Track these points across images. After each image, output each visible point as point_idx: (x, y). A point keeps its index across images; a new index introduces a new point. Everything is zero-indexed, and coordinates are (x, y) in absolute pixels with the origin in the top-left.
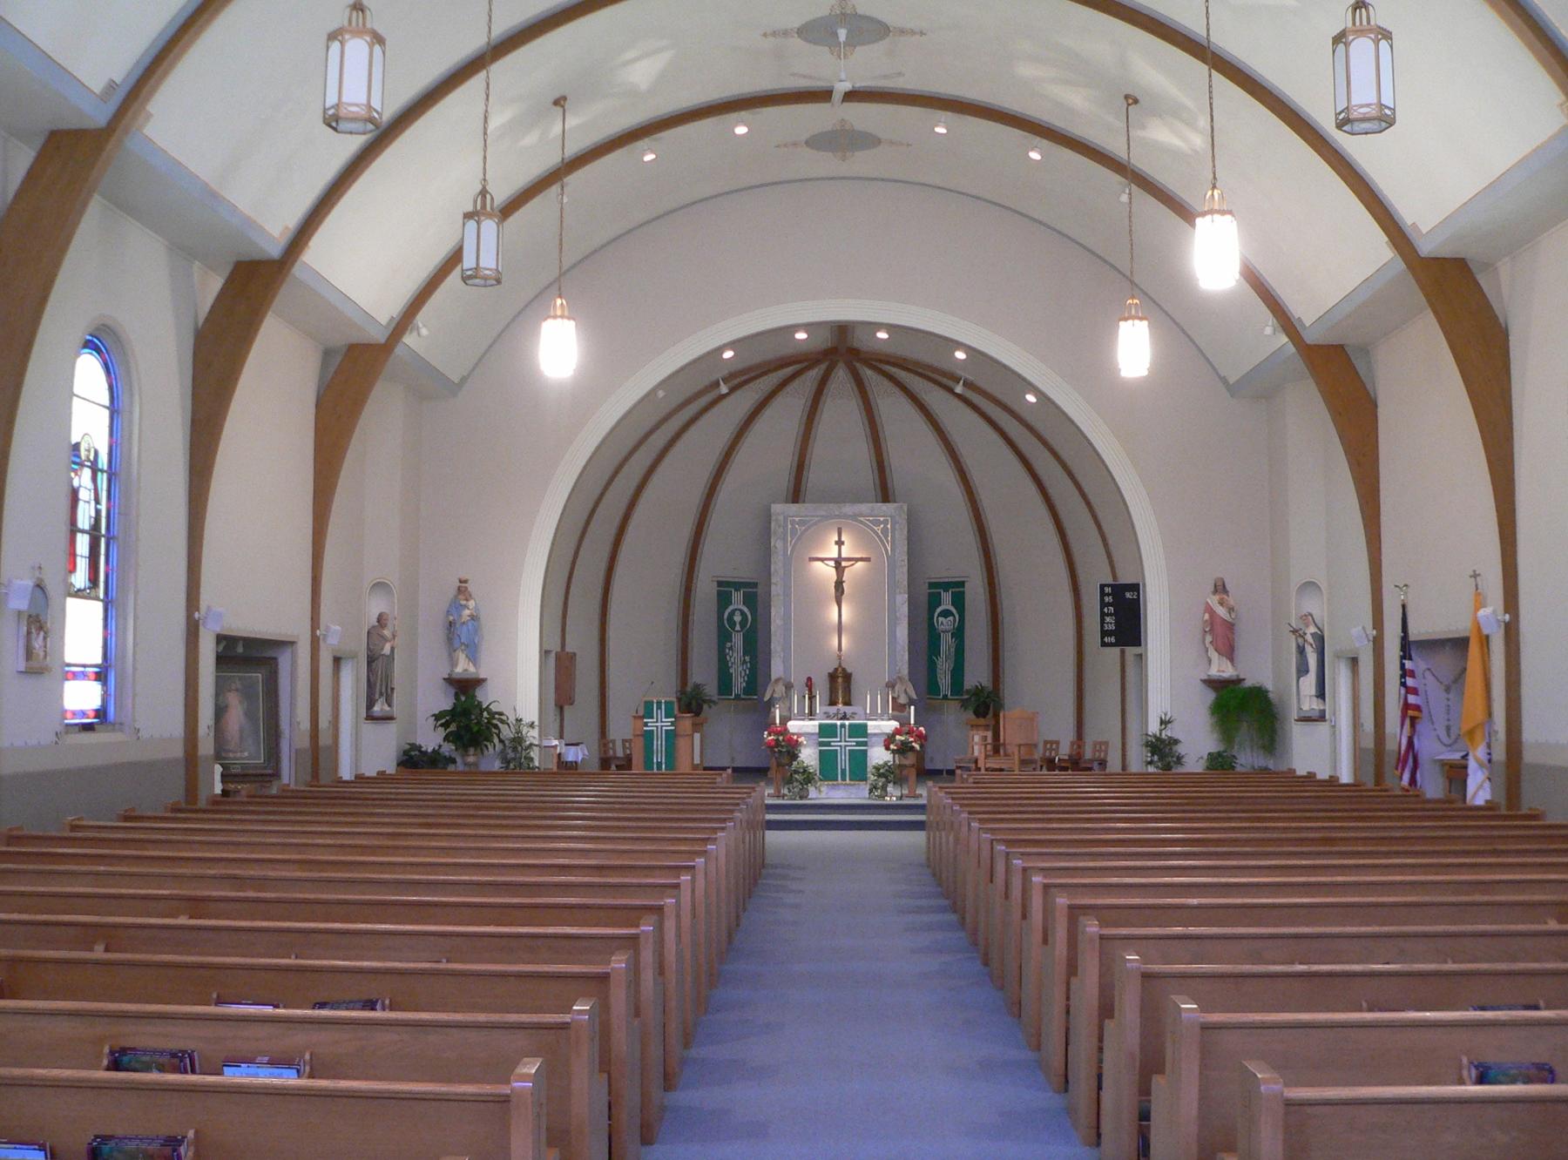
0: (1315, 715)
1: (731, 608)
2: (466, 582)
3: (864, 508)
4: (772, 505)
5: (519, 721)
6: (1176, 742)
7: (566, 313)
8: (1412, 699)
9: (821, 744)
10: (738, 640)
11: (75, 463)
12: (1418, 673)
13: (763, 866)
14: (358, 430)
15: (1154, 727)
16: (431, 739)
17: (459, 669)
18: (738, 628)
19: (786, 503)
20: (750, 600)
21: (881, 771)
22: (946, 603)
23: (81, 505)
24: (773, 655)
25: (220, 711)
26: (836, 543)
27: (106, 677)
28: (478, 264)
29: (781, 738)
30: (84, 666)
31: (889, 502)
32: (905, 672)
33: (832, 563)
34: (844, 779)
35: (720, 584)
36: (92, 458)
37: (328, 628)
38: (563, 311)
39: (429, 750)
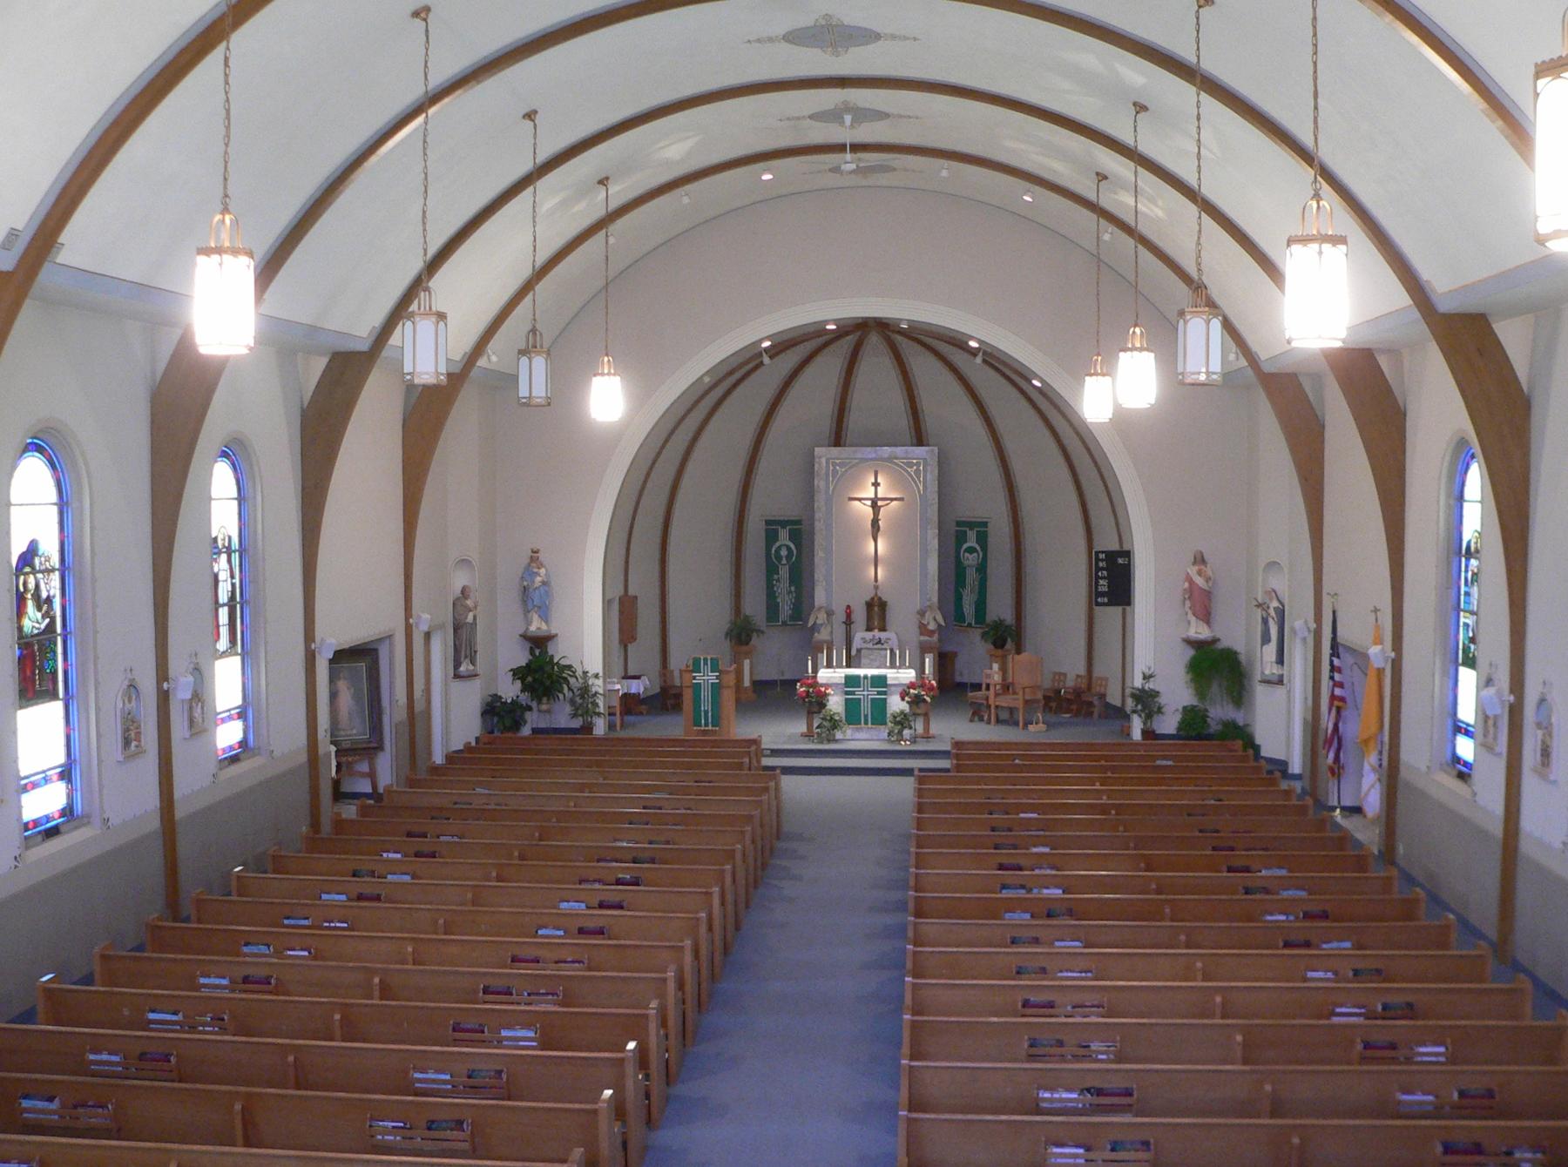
0: (1275, 679)
1: (778, 544)
2: (537, 552)
3: (899, 450)
4: (816, 449)
5: (585, 673)
6: (1157, 694)
7: (612, 371)
8: (1338, 692)
9: (847, 693)
10: (784, 572)
11: (215, 554)
12: (1346, 671)
13: (779, 835)
14: (438, 451)
15: (1138, 682)
16: (510, 690)
17: (533, 628)
18: (784, 561)
19: (829, 446)
20: (796, 536)
21: (898, 719)
22: (972, 542)
23: (221, 585)
24: (816, 583)
25: (333, 696)
26: (873, 484)
27: (246, 713)
28: (530, 394)
29: (811, 690)
30: (229, 710)
31: (922, 445)
32: (935, 599)
33: (869, 503)
34: (866, 723)
35: (768, 522)
36: (227, 545)
37: (419, 617)
38: (610, 368)
39: (509, 701)
